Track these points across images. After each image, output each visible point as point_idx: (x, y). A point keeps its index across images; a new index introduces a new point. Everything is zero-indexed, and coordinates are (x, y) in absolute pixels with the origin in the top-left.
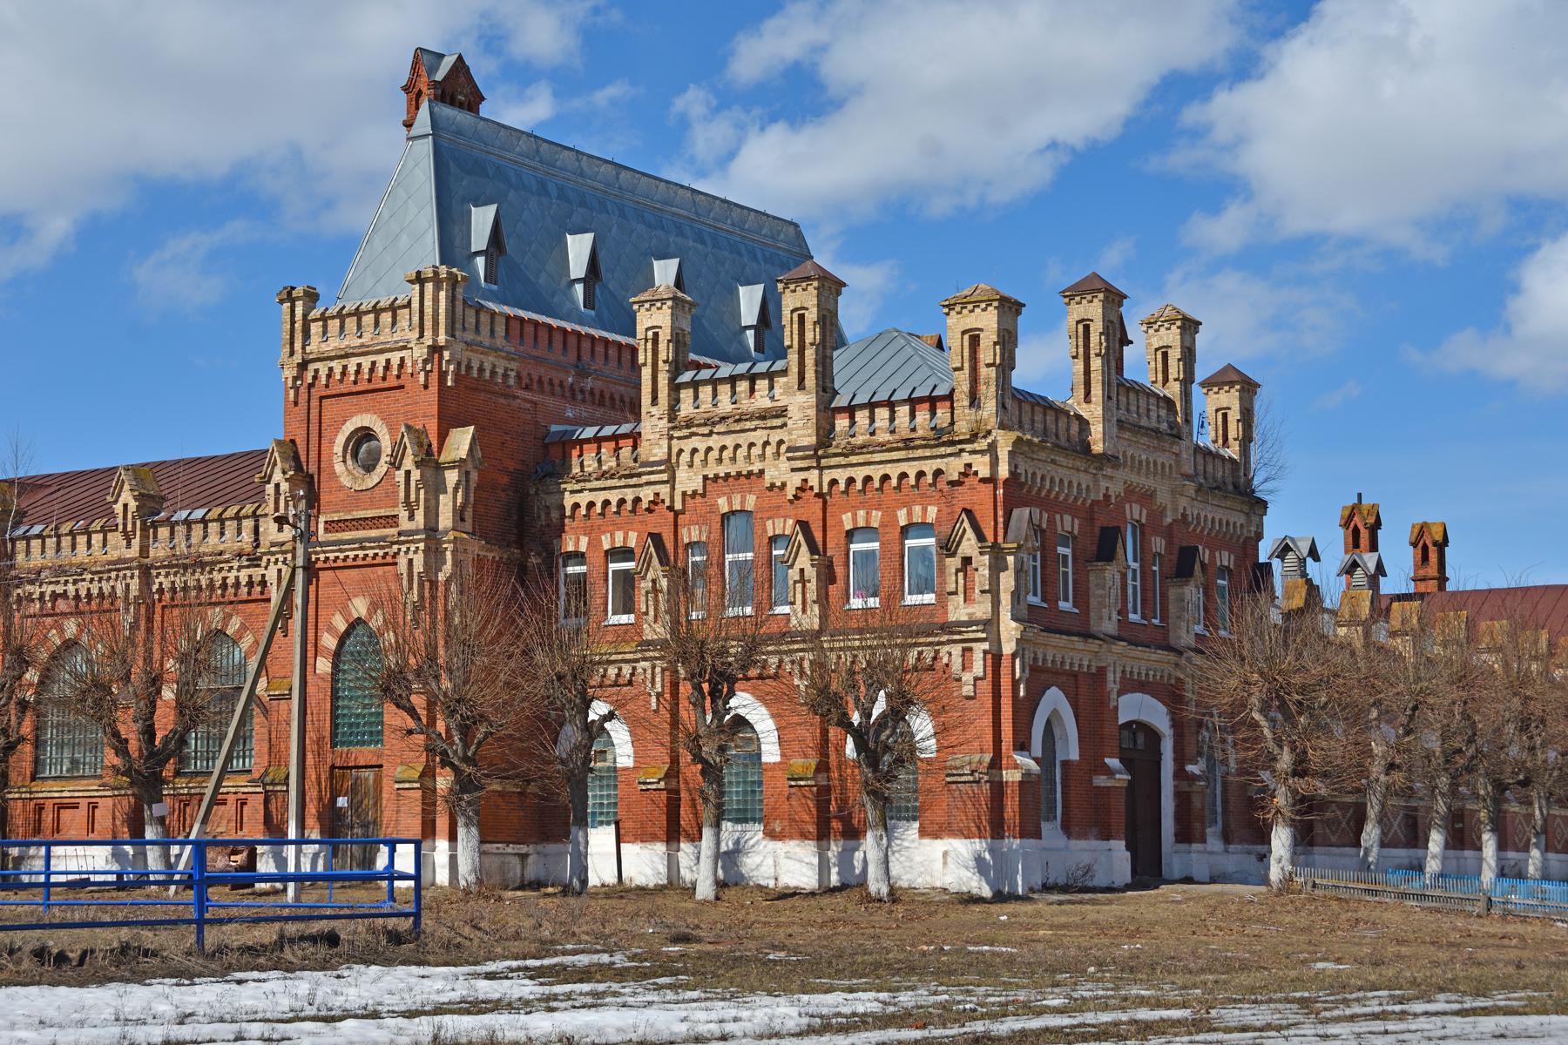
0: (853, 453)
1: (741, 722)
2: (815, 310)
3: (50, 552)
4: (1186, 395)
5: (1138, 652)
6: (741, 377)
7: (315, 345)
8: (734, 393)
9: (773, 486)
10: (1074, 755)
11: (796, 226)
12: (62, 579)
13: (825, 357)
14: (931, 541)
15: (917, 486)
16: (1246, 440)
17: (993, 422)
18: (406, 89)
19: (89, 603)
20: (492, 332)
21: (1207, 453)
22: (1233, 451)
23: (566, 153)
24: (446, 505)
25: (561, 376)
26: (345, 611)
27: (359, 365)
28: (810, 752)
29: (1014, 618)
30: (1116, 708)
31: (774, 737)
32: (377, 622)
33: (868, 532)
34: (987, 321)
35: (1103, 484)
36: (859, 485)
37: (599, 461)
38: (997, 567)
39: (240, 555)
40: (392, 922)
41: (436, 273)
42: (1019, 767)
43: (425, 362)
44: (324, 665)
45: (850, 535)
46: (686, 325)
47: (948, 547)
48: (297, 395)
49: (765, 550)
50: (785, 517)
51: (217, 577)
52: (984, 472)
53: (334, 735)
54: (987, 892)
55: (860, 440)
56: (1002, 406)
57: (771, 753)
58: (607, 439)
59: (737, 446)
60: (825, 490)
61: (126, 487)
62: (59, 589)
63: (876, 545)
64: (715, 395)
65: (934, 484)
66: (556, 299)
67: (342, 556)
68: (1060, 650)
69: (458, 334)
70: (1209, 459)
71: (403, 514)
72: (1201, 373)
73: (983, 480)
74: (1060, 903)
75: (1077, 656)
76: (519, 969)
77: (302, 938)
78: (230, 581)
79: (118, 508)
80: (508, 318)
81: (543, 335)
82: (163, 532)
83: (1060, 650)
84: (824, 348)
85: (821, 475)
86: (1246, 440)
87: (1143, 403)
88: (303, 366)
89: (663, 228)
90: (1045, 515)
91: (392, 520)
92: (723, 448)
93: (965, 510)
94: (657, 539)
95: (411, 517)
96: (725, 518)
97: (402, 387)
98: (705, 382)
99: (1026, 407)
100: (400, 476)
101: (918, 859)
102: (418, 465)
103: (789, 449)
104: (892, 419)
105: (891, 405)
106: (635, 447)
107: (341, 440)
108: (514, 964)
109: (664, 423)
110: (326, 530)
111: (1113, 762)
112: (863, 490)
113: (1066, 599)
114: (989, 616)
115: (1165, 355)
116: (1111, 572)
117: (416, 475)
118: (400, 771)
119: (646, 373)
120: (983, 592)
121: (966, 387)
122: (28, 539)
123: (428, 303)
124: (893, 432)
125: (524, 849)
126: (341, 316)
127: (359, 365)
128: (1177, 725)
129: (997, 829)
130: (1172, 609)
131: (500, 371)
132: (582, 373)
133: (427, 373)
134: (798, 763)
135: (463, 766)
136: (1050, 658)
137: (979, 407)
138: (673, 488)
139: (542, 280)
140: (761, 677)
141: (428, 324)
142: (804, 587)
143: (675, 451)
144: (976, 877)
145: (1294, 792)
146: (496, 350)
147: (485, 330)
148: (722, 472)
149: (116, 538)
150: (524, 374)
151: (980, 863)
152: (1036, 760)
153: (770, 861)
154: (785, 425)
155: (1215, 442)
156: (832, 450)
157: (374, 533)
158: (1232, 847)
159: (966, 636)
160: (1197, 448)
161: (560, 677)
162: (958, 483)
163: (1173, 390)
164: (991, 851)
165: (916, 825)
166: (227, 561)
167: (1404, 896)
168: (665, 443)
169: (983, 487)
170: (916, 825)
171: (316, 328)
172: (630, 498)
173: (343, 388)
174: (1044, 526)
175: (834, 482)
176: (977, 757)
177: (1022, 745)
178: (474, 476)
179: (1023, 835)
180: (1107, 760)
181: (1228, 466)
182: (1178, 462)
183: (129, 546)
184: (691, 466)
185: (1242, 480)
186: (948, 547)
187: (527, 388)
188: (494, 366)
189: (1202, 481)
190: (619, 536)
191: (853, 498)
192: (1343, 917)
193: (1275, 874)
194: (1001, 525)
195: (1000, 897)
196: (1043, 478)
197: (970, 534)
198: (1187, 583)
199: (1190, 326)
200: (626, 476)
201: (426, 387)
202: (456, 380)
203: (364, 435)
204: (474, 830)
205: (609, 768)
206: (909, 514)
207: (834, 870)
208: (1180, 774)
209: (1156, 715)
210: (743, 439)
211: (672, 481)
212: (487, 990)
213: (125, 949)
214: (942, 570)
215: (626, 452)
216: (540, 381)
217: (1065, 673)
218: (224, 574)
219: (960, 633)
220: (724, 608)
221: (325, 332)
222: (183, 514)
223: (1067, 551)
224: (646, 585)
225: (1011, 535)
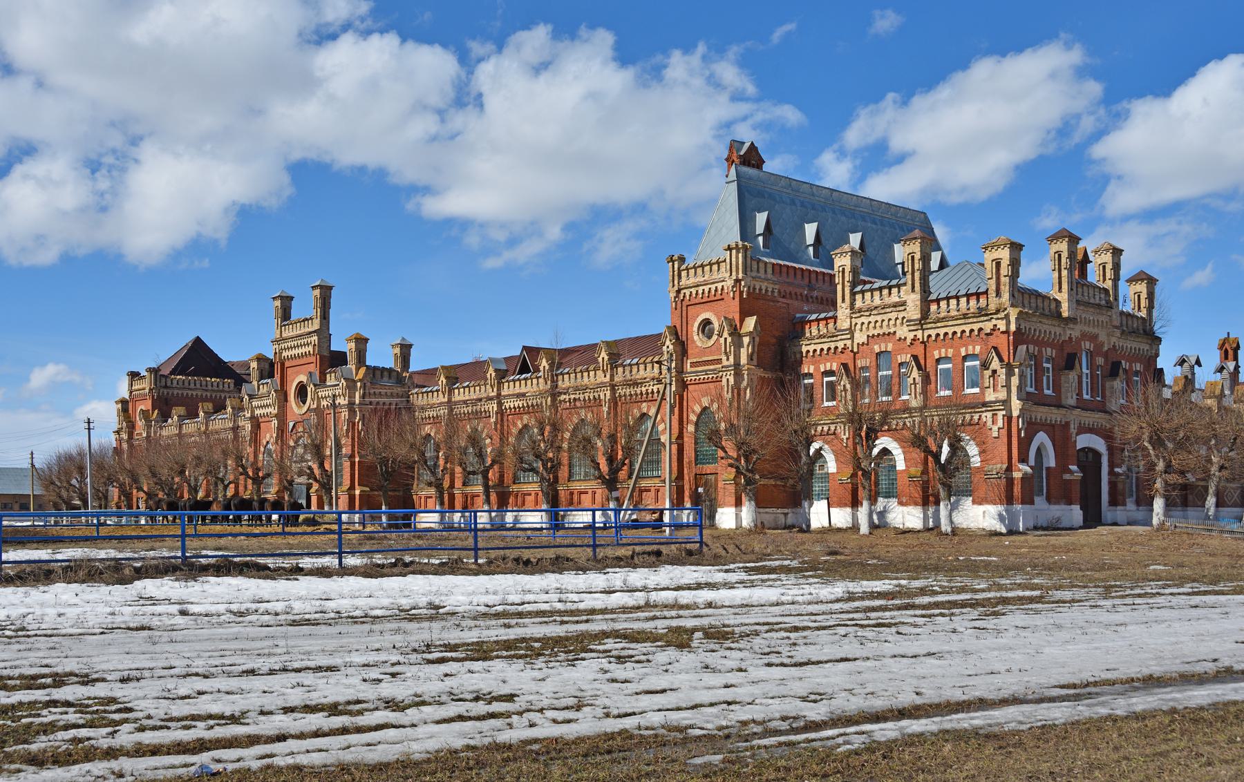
0: (939, 322)
1: (885, 451)
2: (919, 253)
3: (573, 380)
4: (1115, 286)
5: (1088, 414)
6: (884, 287)
7: (684, 282)
8: (881, 295)
9: (900, 339)
10: (1052, 464)
11: (925, 213)
12: (578, 392)
13: (925, 276)
14: (978, 363)
15: (970, 336)
16: (1150, 307)
17: (1008, 304)
18: (727, 160)
19: (589, 402)
20: (766, 271)
21: (1128, 315)
22: (1143, 314)
23: (805, 185)
24: (744, 354)
25: (802, 291)
26: (700, 403)
27: (703, 290)
28: (919, 465)
30: (1076, 441)
31: (902, 457)
34: (1004, 254)
35: (1068, 332)
36: (942, 337)
37: (819, 330)
38: (1010, 374)
39: (653, 379)
40: (688, 546)
41: (737, 245)
42: (1021, 470)
43: (733, 287)
44: (691, 428)
45: (938, 361)
46: (858, 264)
47: (985, 366)
48: (676, 305)
49: (897, 370)
50: (907, 353)
51: (644, 389)
52: (1003, 328)
53: (696, 459)
54: (1004, 530)
55: (942, 315)
56: (1012, 296)
57: (901, 465)
58: (822, 319)
59: (883, 321)
60: (925, 340)
61: (603, 350)
62: (577, 396)
63: (950, 366)
64: (872, 297)
65: (978, 335)
66: (799, 254)
67: (698, 378)
68: (1042, 413)
69: (748, 273)
70: (1129, 318)
71: (724, 358)
72: (1125, 273)
73: (1003, 332)
74: (1041, 535)
75: (1054, 417)
76: (743, 568)
77: (644, 553)
80: (773, 264)
81: (791, 272)
82: (620, 370)
83: (1042, 413)
84: (924, 271)
85: (923, 333)
86: (1150, 307)
87: (1091, 292)
88: (678, 292)
89: (854, 218)
90: (1037, 348)
92: (876, 322)
94: (845, 366)
95: (728, 359)
97: (723, 299)
98: (867, 291)
99: (1026, 296)
100: (722, 340)
101: (971, 515)
102: (730, 335)
103: (907, 321)
104: (958, 305)
105: (957, 297)
106: (835, 323)
107: (696, 325)
108: (741, 565)
110: (691, 366)
111: (1074, 468)
112: (944, 339)
113: (1048, 389)
114: (1005, 398)
115: (1104, 267)
116: (1072, 375)
117: (729, 340)
119: (839, 288)
120: (1002, 386)
121: (994, 287)
122: (624, 366)
123: (734, 259)
124: (958, 311)
125: (786, 511)
126: (695, 268)
127: (703, 290)
128: (1110, 449)
129: (1009, 500)
130: (1108, 394)
131: (770, 290)
132: (811, 288)
133: (734, 292)
134: (913, 470)
135: (747, 474)
136: (1039, 418)
137: (1000, 297)
138: (853, 342)
139: (792, 246)
140: (889, 430)
142: (915, 386)
143: (853, 324)
144: (999, 523)
145: (1166, 482)
146: (768, 280)
147: (762, 271)
149: (600, 373)
150: (782, 291)
151: (1001, 518)
152: (1031, 467)
153: (900, 516)
154: (905, 309)
155: (1134, 309)
156: (928, 321)
157: (712, 367)
158: (1141, 508)
159: (994, 408)
160: (1122, 313)
161: (795, 432)
162: (990, 334)
163: (1108, 284)
164: (1006, 511)
165: (971, 498)
166: (648, 382)
167: (1222, 532)
168: (848, 320)
169: (1003, 335)
170: (971, 498)
171: (684, 274)
172: (833, 347)
174: (1036, 354)
175: (929, 336)
176: (999, 466)
177: (1023, 459)
178: (757, 339)
179: (1022, 503)
181: (1140, 321)
182: (1111, 321)
184: (861, 331)
185: (1148, 327)
186: (985, 366)
187: (784, 297)
188: (767, 288)
189: (1125, 329)
191: (939, 344)
192: (1188, 542)
193: (1155, 521)
194: (1011, 354)
195: (1011, 532)
196: (1035, 330)
197: (996, 358)
198: (1115, 379)
199: (1117, 252)
200: (831, 337)
201: (734, 299)
202: (747, 295)
203: (707, 322)
204: (753, 503)
205: (825, 474)
206: (967, 350)
207: (931, 520)
208: (1111, 473)
209: (1099, 444)
210: (886, 317)
211: (852, 338)
212: (719, 577)
213: (558, 558)
214: (982, 377)
215: (831, 325)
216: (790, 293)
217: (1047, 425)
218: (647, 388)
219: (991, 407)
220: (878, 397)
221: (688, 276)
222: (628, 361)
223: (1049, 366)
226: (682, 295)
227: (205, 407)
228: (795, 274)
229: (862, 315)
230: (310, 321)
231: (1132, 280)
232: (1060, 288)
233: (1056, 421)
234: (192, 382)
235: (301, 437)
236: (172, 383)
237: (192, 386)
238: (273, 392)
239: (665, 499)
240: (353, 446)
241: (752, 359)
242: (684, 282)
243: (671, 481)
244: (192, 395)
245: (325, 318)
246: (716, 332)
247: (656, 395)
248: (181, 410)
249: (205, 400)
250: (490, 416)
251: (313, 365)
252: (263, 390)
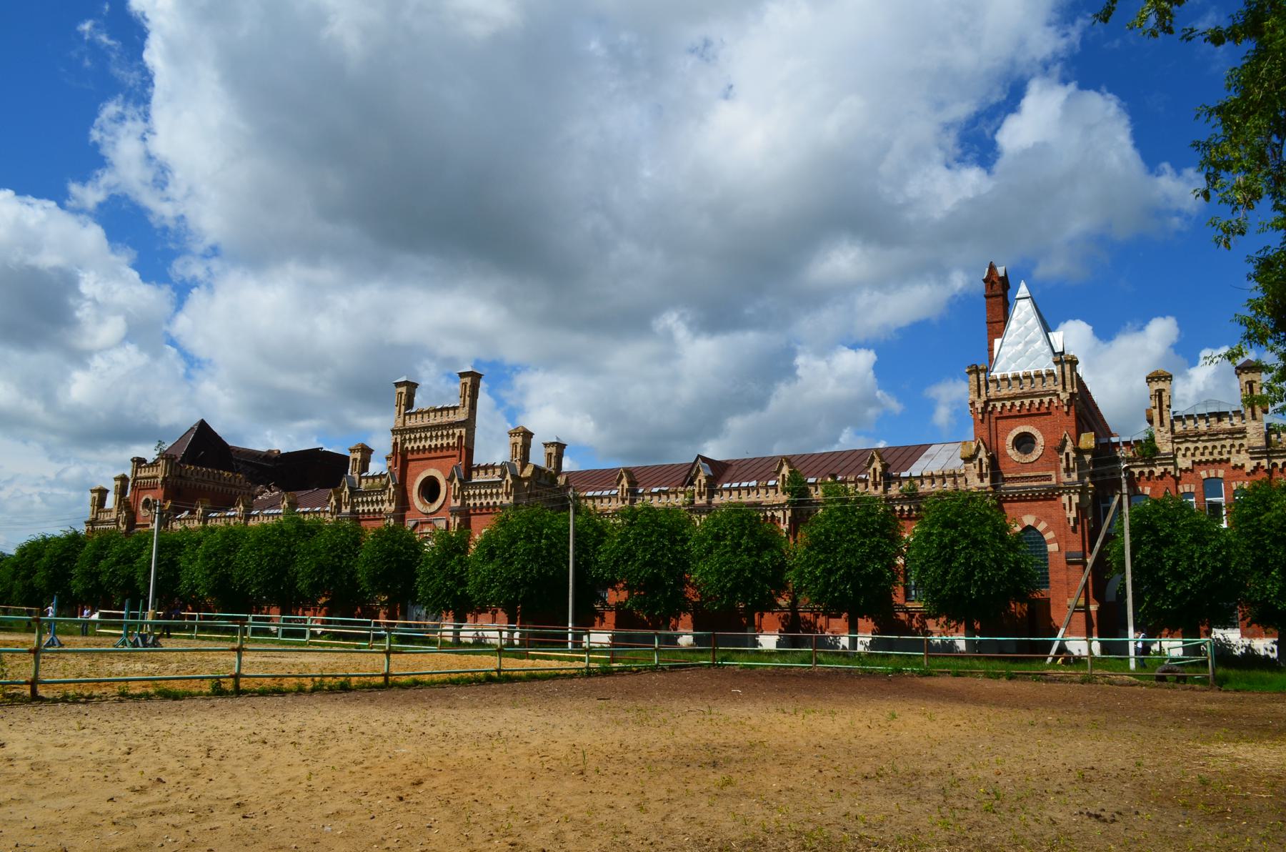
7: (139, 475)
18: (985, 281)
32: (1041, 527)
88: (986, 403)
97: (1050, 414)
109: (1169, 435)
148: (1204, 459)
154: (1245, 437)
242: (139, 475)
244: (200, 486)
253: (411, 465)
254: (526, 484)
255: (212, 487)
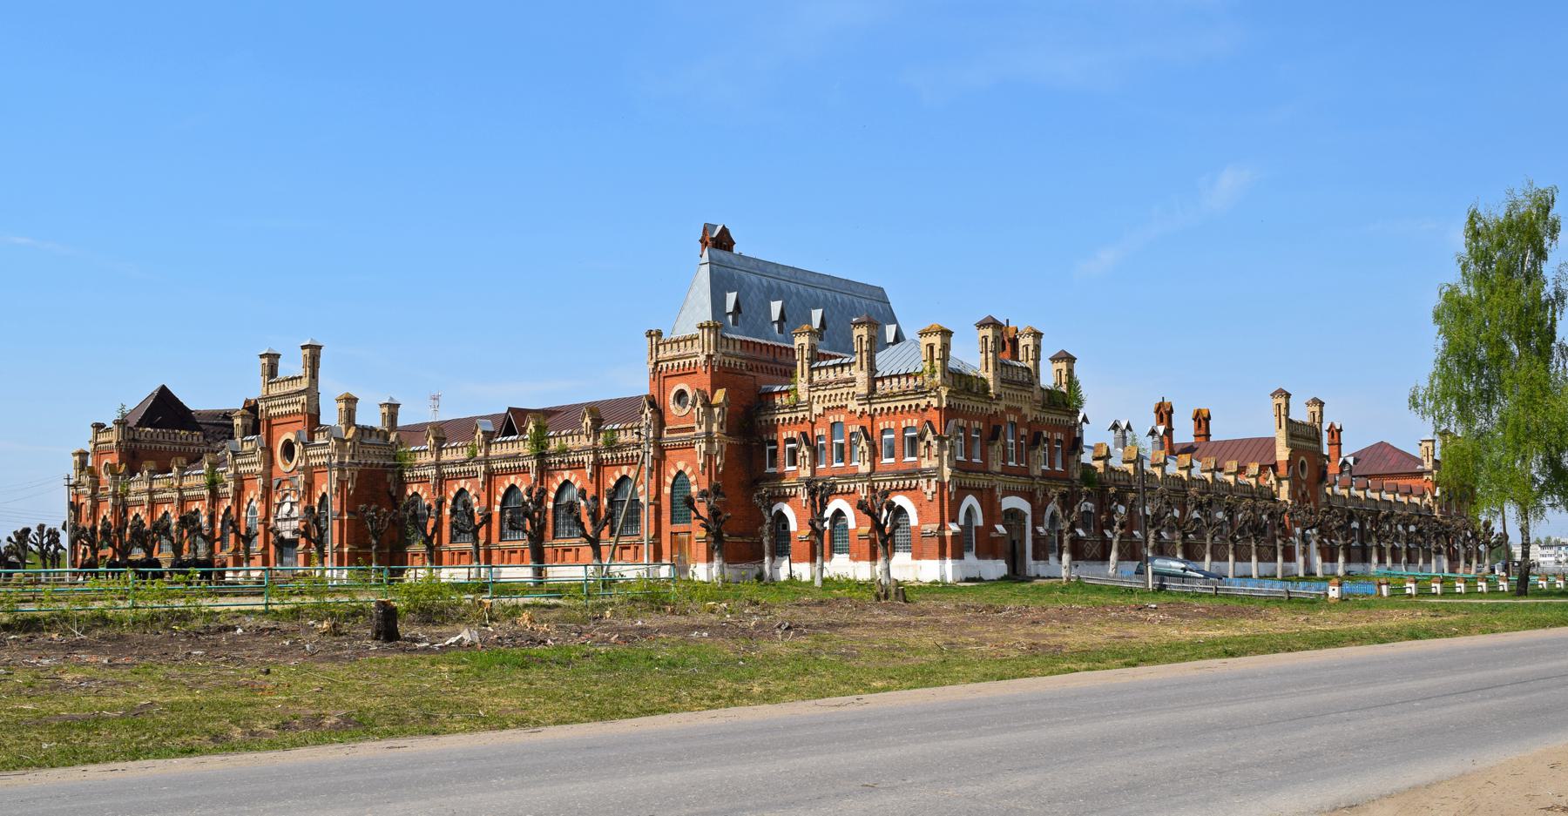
4: (1037, 366)
7: (98, 440)
8: (835, 372)
18: (701, 241)
20: (734, 346)
29: (949, 467)
33: (890, 430)
34: (936, 340)
35: (994, 407)
38: (941, 447)
41: (709, 324)
43: (705, 361)
45: (883, 432)
48: (654, 376)
49: (848, 438)
50: (857, 424)
52: (935, 405)
56: (944, 376)
64: (827, 373)
68: (969, 480)
71: (697, 427)
73: (935, 408)
78: (629, 455)
79: (584, 425)
80: (741, 341)
81: (758, 347)
83: (969, 480)
85: (870, 408)
88: (656, 364)
90: (966, 422)
91: (692, 429)
93: (927, 421)
95: (700, 427)
96: (833, 424)
100: (695, 411)
102: (702, 405)
104: (899, 382)
107: (672, 394)
115: (1027, 349)
118: (698, 534)
119: (799, 363)
123: (706, 336)
126: (671, 342)
128: (1033, 509)
131: (738, 364)
138: (811, 413)
141: (706, 345)
147: (731, 347)
149: (583, 437)
150: (749, 364)
152: (960, 527)
157: (686, 434)
163: (1031, 364)
168: (807, 393)
171: (661, 348)
173: (673, 373)
175: (875, 410)
177: (954, 520)
178: (726, 409)
180: (996, 526)
183: (588, 440)
187: (751, 370)
190: (790, 433)
197: (930, 431)
201: (706, 372)
206: (906, 423)
208: (1034, 531)
209: (1023, 505)
210: (839, 392)
211: (810, 410)
216: (757, 367)
220: (832, 464)
224: (800, 454)
225: (947, 431)
226: (659, 367)
227: (179, 462)
228: (761, 349)
229: (818, 390)
230: (298, 380)
231: (1054, 359)
232: (987, 368)
233: (983, 485)
234: (166, 435)
235: (287, 495)
236: (140, 436)
237: (161, 438)
238: (258, 449)
239: (643, 555)
240: (342, 504)
241: (722, 428)
242: (98, 440)
243: (648, 540)
244: (160, 448)
245: (314, 377)
246: (690, 402)
247: (635, 459)
248: (152, 465)
249: (180, 454)
250: (477, 476)
251: (302, 423)
252: (248, 447)
253: (276, 429)
254: (348, 444)
255: (168, 447)
